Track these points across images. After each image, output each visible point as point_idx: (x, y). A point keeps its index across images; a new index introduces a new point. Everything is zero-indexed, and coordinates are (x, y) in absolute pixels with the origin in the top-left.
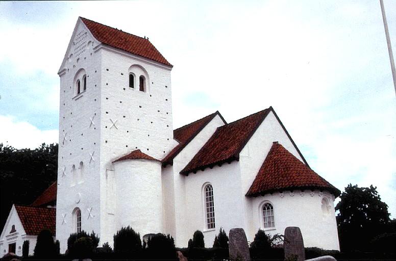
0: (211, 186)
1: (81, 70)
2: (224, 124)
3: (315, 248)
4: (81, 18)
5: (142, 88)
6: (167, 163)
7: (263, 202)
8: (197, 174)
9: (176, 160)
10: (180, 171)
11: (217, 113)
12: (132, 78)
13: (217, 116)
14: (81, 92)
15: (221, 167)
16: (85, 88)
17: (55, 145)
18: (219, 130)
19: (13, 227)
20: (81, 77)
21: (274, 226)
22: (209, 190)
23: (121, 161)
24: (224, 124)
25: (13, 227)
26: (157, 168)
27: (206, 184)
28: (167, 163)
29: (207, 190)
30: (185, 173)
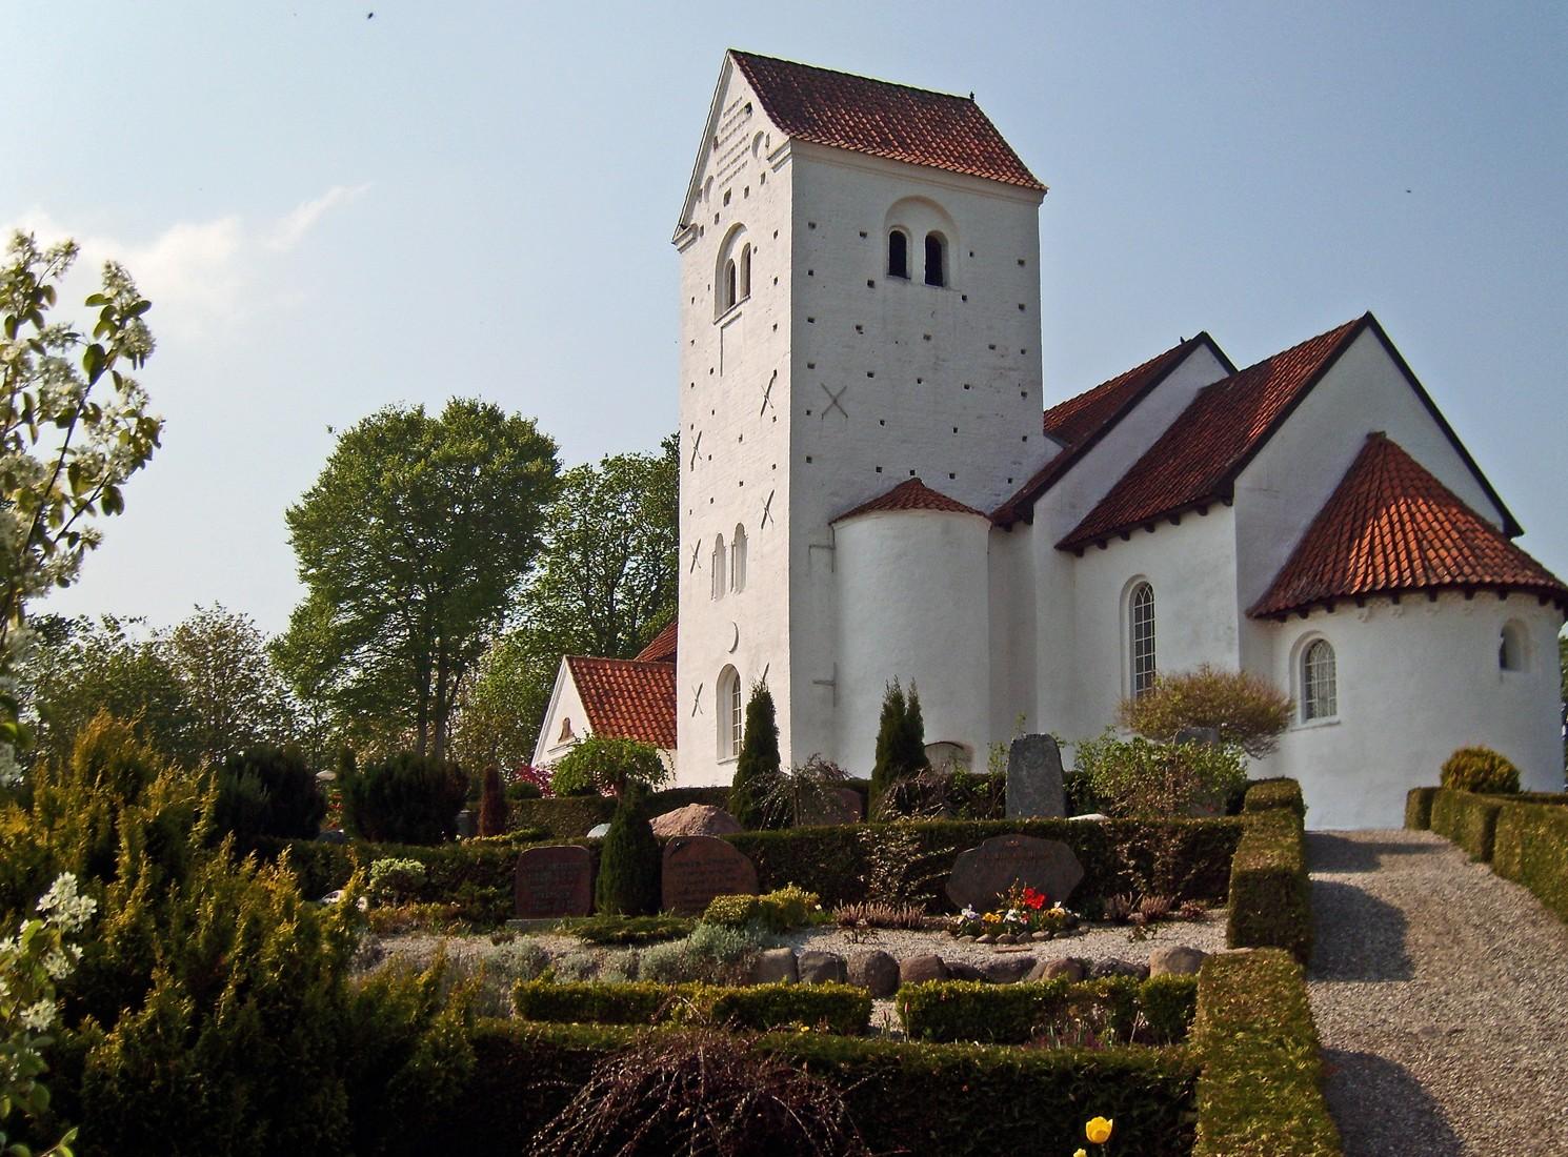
0: (1151, 589)
1: (737, 229)
2: (1226, 375)
3: (879, 739)
4: (733, 52)
5: (935, 274)
6: (1012, 518)
7: (1299, 642)
8: (1086, 555)
9: (1042, 506)
10: (1055, 544)
11: (1368, 321)
12: (898, 243)
13: (1367, 337)
14: (737, 300)
15: (1179, 527)
16: (748, 292)
17: (114, 514)
18: (1207, 395)
19: (567, 723)
20: (736, 254)
21: (1334, 713)
22: (1142, 597)
23: (855, 519)
24: (1226, 375)
25: (567, 723)
26: (976, 531)
27: (1136, 583)
28: (1012, 518)
29: (1138, 602)
30: (1075, 545)
